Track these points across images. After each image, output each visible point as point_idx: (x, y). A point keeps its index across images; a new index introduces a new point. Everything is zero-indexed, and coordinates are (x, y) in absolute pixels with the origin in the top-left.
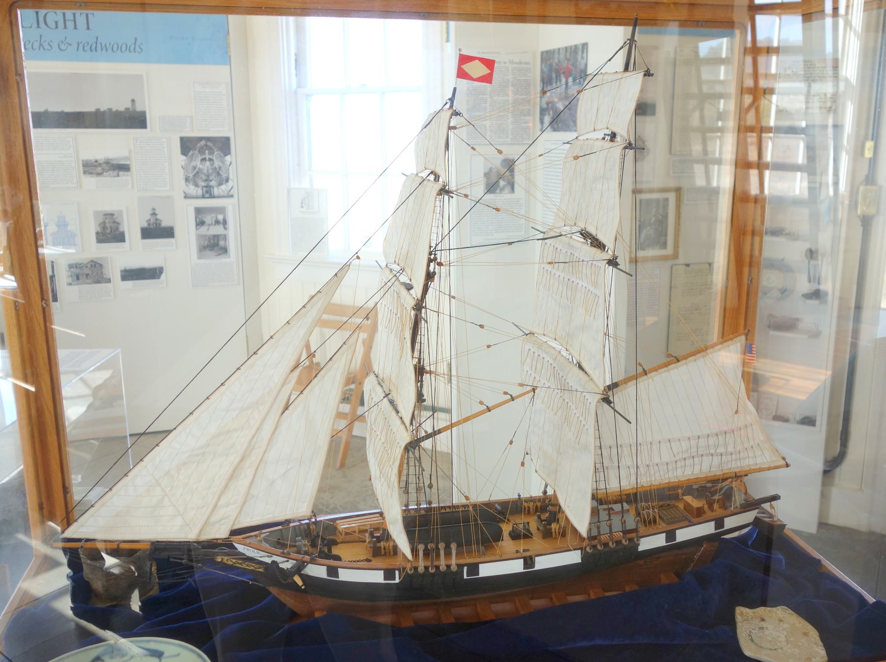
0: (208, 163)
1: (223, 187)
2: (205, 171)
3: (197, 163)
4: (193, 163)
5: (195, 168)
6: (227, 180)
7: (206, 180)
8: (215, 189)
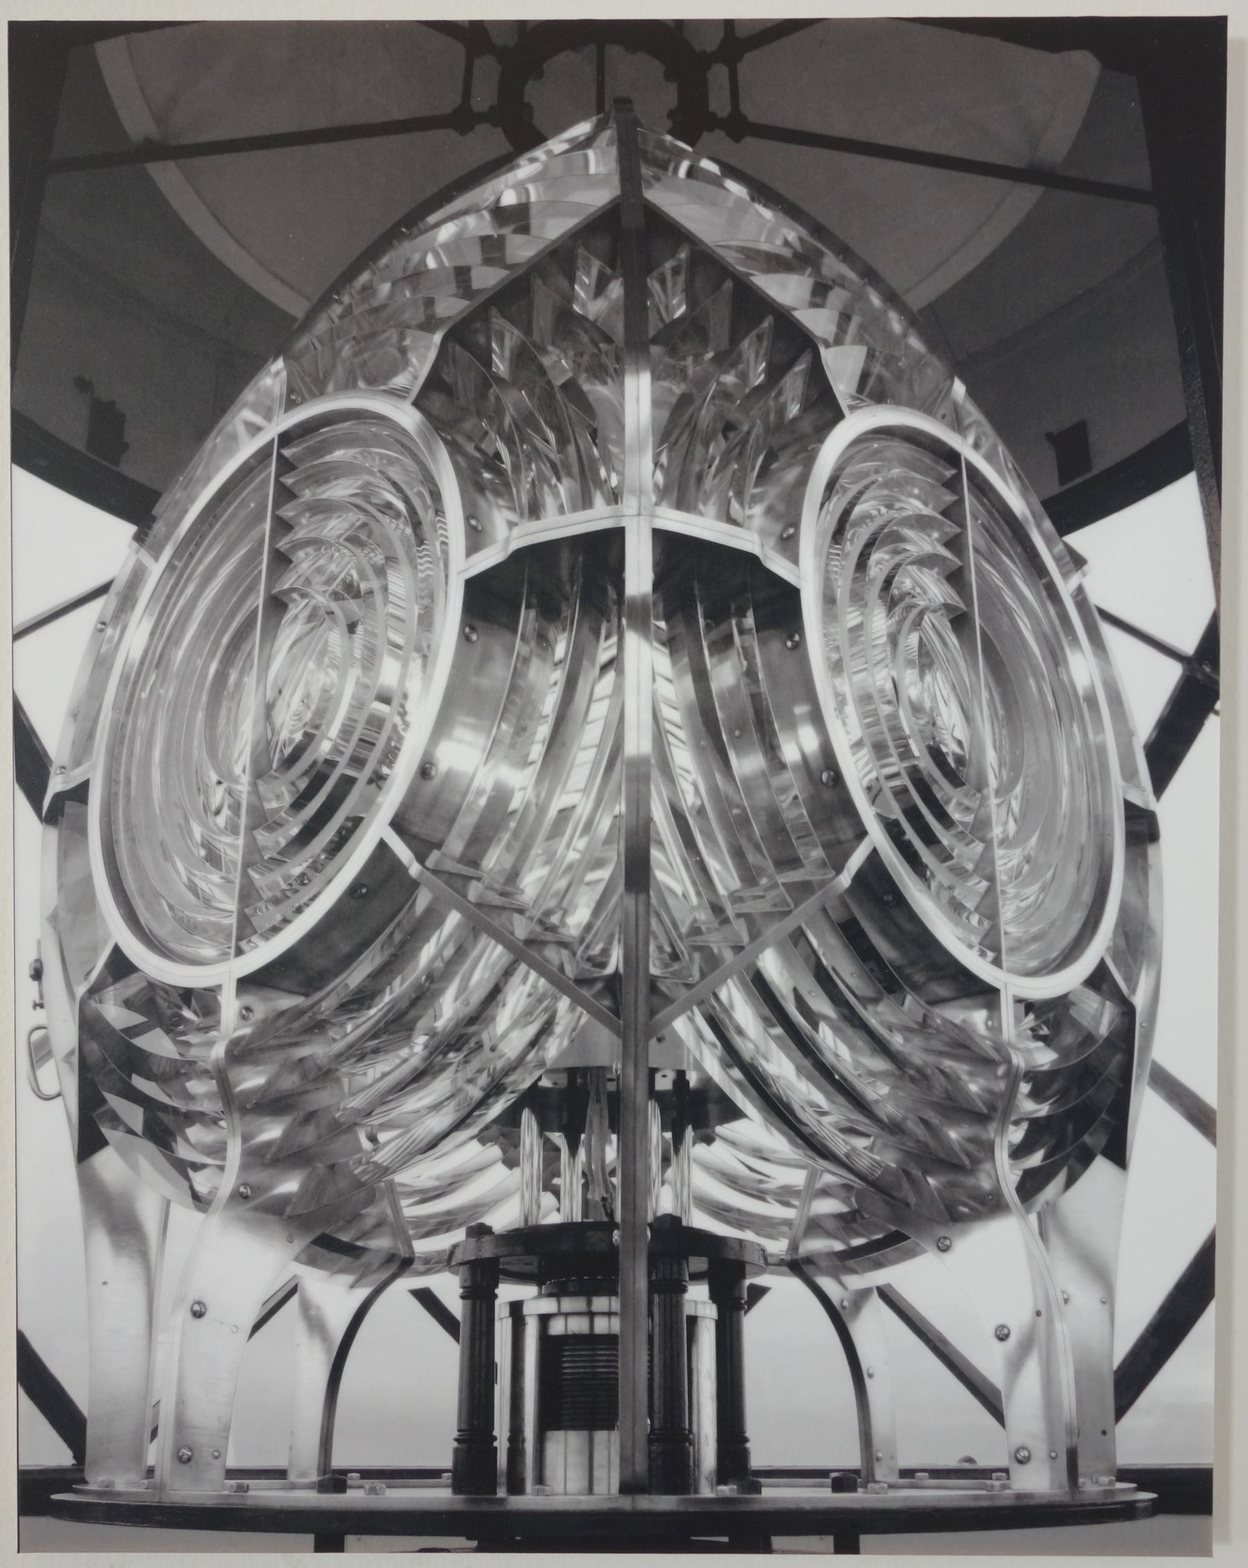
0: (644, 679)
1: (977, 1277)
2: (567, 883)
3: (392, 673)
4: (303, 682)
5: (320, 791)
6: (1087, 1110)
7: (568, 1104)
8: (784, 1319)
